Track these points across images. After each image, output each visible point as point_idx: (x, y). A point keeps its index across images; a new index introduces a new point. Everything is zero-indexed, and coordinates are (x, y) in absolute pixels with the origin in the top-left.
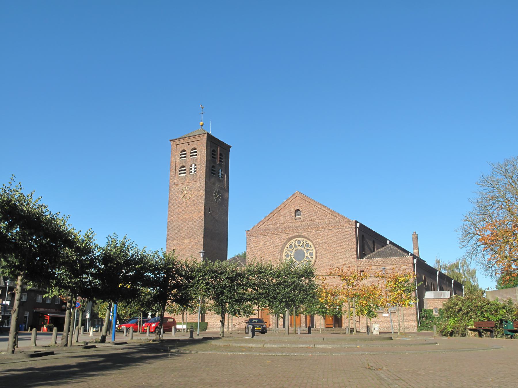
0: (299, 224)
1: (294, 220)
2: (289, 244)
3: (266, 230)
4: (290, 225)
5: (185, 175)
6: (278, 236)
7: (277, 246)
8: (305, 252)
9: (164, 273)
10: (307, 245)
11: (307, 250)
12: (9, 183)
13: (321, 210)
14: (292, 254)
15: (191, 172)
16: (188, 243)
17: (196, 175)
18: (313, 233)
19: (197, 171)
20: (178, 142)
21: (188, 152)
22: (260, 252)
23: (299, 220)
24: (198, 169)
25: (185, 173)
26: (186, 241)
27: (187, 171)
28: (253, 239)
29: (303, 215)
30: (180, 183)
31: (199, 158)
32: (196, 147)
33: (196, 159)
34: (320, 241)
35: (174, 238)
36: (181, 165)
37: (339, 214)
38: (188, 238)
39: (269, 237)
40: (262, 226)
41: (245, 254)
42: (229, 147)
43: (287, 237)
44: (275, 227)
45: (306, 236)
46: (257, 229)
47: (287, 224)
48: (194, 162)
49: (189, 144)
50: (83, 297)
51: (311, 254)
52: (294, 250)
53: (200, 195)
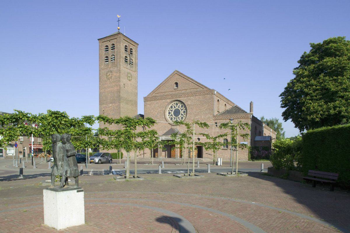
0: (177, 92)
3: (156, 97)
4: (171, 93)
6: (164, 101)
8: (180, 110)
13: (191, 83)
16: (111, 106)
18: (185, 98)
21: (110, 46)
26: (110, 105)
28: (148, 103)
37: (203, 85)
38: (111, 103)
39: (158, 101)
40: (154, 94)
44: (162, 94)
46: (151, 96)
47: (170, 93)
48: (113, 54)
51: (169, 113)
52: (173, 110)
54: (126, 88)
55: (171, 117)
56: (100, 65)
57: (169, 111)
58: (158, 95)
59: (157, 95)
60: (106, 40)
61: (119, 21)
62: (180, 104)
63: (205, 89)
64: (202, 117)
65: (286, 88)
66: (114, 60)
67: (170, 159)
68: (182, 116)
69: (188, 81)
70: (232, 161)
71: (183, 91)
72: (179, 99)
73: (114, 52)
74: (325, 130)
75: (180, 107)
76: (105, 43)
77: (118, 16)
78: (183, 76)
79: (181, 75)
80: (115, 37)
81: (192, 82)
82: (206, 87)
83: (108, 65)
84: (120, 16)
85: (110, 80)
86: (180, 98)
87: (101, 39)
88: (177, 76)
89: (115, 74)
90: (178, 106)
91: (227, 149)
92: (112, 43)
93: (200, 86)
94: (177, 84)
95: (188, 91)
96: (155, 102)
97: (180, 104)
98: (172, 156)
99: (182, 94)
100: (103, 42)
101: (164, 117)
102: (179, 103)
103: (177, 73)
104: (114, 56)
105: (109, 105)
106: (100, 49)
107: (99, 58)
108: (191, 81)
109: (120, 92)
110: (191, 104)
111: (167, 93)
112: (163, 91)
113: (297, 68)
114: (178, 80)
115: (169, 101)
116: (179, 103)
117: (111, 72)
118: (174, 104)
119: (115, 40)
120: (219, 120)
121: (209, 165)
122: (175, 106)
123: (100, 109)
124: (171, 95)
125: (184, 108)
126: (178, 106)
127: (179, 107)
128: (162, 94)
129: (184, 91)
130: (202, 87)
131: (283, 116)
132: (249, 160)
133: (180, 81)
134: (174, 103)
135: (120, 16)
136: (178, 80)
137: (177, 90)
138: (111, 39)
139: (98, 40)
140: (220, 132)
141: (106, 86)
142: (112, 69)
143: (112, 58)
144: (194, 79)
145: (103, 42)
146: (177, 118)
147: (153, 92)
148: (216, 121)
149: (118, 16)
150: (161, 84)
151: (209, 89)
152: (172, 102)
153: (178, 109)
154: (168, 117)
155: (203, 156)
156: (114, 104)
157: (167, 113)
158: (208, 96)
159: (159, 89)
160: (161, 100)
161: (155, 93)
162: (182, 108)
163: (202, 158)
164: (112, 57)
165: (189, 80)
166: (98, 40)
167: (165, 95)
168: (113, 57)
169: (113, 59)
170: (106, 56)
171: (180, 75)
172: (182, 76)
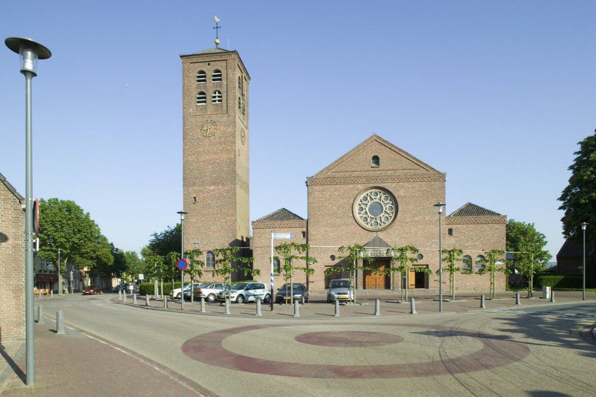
0: (377, 172)
4: (366, 174)
5: (204, 104)
6: (350, 186)
7: (349, 198)
8: (383, 205)
9: (61, 251)
12: (64, 293)
13: (405, 159)
16: (214, 190)
18: (394, 185)
20: (195, 60)
21: (210, 74)
22: (326, 204)
25: (205, 102)
26: (212, 188)
30: (198, 114)
34: (402, 195)
35: (194, 184)
37: (427, 165)
38: (214, 184)
39: (339, 186)
40: (329, 174)
41: (179, 229)
44: (347, 175)
46: (323, 176)
47: (362, 173)
48: (218, 89)
49: (209, 64)
50: (586, 231)
52: (369, 204)
56: (184, 108)
57: (359, 205)
59: (337, 175)
60: (200, 60)
61: (217, 28)
62: (382, 193)
63: (431, 172)
66: (219, 101)
67: (387, 291)
68: (387, 215)
69: (398, 155)
70: (492, 291)
71: (389, 172)
72: (381, 185)
73: (221, 85)
75: (382, 199)
76: (196, 64)
77: (216, 17)
78: (390, 147)
79: (386, 144)
80: (224, 58)
81: (408, 157)
82: (433, 169)
83: (205, 108)
84: (219, 20)
85: (212, 139)
87: (188, 56)
88: (378, 146)
89: (223, 128)
90: (378, 197)
91: (278, 274)
92: (215, 68)
93: (422, 165)
94: (376, 159)
95: (399, 173)
96: (333, 188)
97: (382, 193)
98: (367, 286)
99: (387, 176)
100: (191, 63)
101: (351, 215)
102: (380, 193)
103: (378, 140)
104: (219, 93)
105: (208, 188)
106: (184, 76)
107: (184, 93)
108: (405, 156)
109: (234, 164)
112: (349, 169)
113: (578, 153)
114: (378, 153)
115: (360, 187)
116: (380, 193)
117: (214, 123)
118: (369, 194)
119: (224, 63)
120: (455, 225)
121: (378, 302)
122: (373, 197)
123: (185, 194)
124: (366, 176)
125: (391, 202)
126: (378, 197)
130: (425, 167)
132: (507, 290)
133: (383, 154)
134: (370, 191)
135: (219, 20)
136: (378, 153)
137: (377, 169)
138: (212, 59)
139: (181, 57)
141: (201, 149)
142: (214, 118)
143: (214, 97)
144: (410, 153)
145: (191, 63)
146: (376, 219)
147: (328, 169)
148: (450, 227)
149: (216, 17)
150: (344, 156)
151: (439, 173)
152: (366, 190)
153: (379, 203)
154: (357, 216)
155: (430, 285)
156: (220, 187)
157: (356, 209)
158: (437, 183)
159: (340, 165)
160: (345, 185)
162: (387, 202)
163: (427, 288)
164: (215, 95)
165: (402, 154)
166: (181, 57)
168: (217, 94)
169: (217, 98)
170: (199, 91)
171: (384, 143)
172: (387, 145)
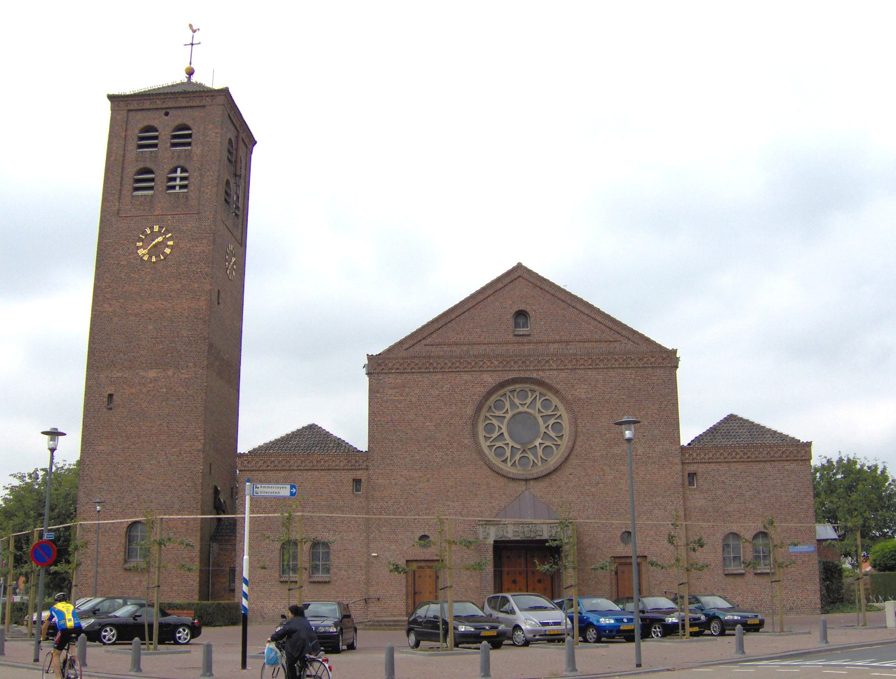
0: (526, 347)
1: (511, 337)
2: (493, 398)
3: (430, 357)
5: (150, 192)
6: (466, 377)
8: (540, 420)
10: (500, 452)
11: (546, 418)
13: (585, 317)
14: (525, 409)
15: (174, 187)
16: (156, 380)
17: (186, 197)
19: (192, 188)
23: (526, 339)
24: (194, 181)
26: (152, 374)
27: (160, 183)
28: (391, 379)
29: (535, 327)
31: (198, 152)
32: (189, 123)
33: (189, 155)
34: (583, 396)
36: (141, 165)
39: (439, 376)
40: (417, 348)
42: (120, 103)
43: (490, 380)
44: (457, 350)
45: (547, 380)
46: (403, 354)
48: (182, 163)
49: (167, 114)
51: (557, 426)
53: (198, 250)
54: (221, 306)
55: (498, 444)
58: (441, 354)
59: (436, 351)
61: (192, 44)
64: (639, 452)
65: (677, 367)
74: (268, 481)
86: (541, 373)
92: (179, 121)
99: (548, 355)
104: (184, 170)
105: (142, 373)
110: (591, 399)
111: (481, 349)
119: (197, 113)
127: (513, 405)
128: (457, 350)
129: (556, 346)
131: (849, 460)
140: (710, 509)
156: (170, 373)
161: (423, 342)
164: (173, 175)
167: (475, 356)
